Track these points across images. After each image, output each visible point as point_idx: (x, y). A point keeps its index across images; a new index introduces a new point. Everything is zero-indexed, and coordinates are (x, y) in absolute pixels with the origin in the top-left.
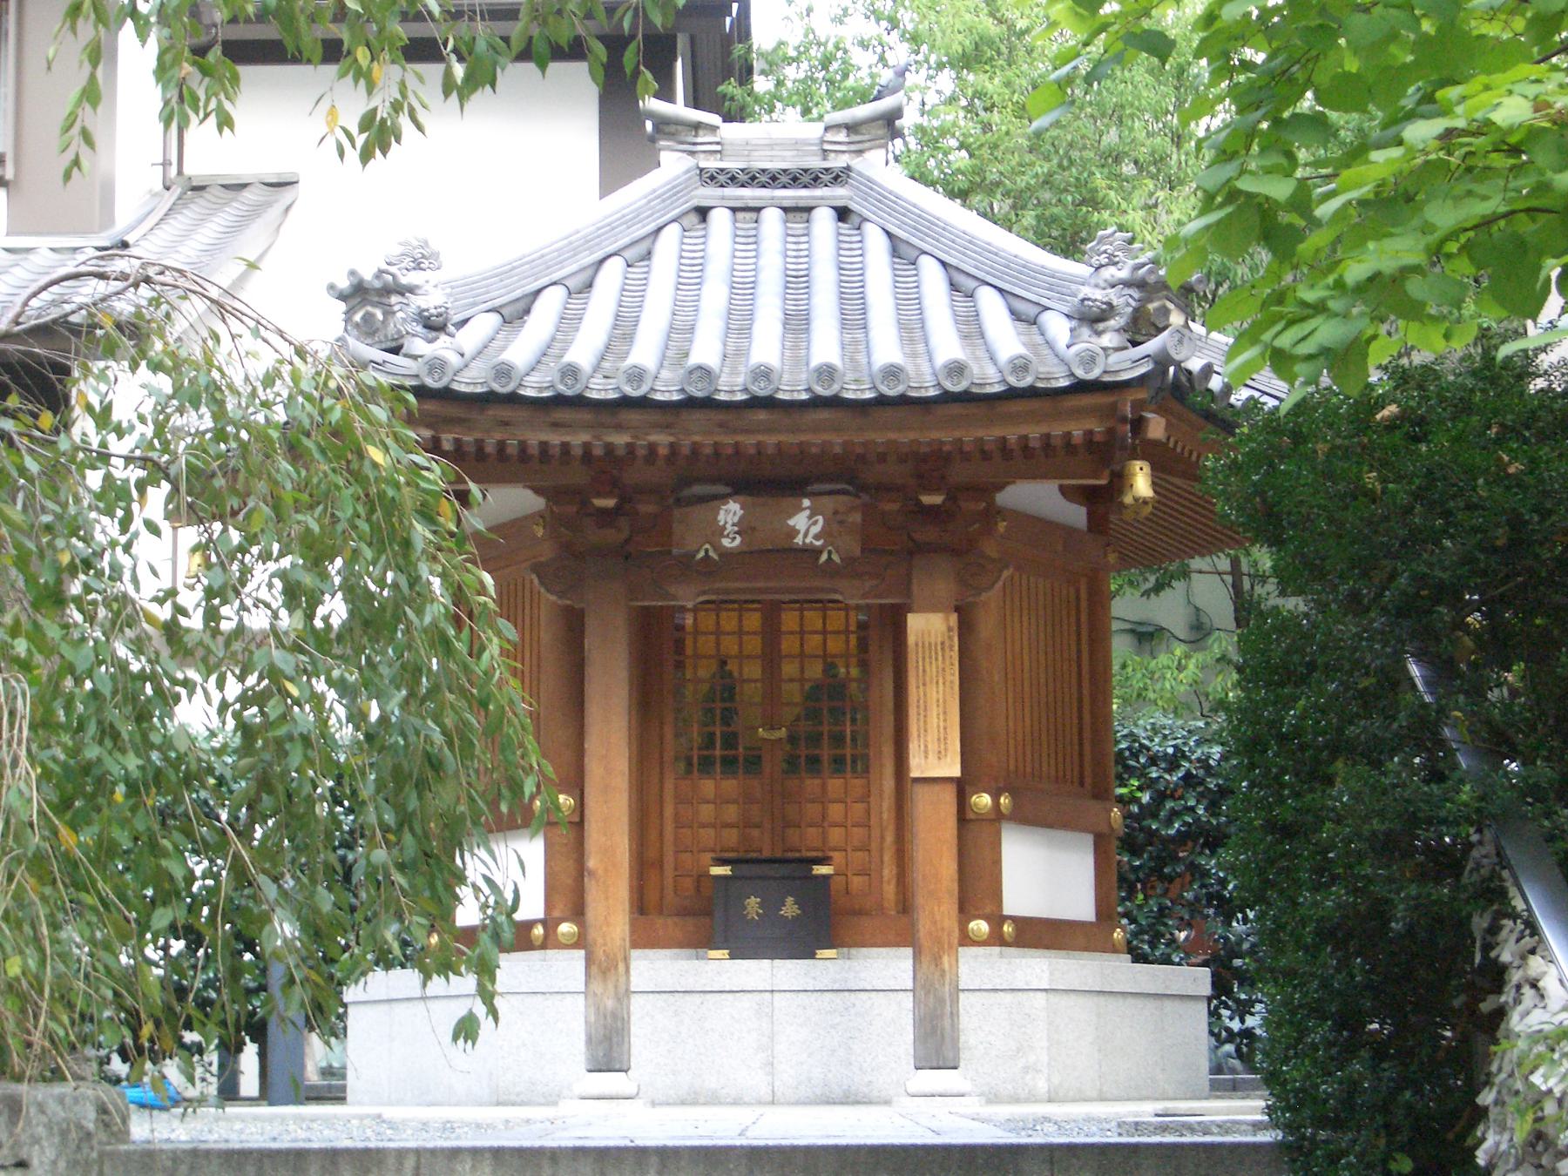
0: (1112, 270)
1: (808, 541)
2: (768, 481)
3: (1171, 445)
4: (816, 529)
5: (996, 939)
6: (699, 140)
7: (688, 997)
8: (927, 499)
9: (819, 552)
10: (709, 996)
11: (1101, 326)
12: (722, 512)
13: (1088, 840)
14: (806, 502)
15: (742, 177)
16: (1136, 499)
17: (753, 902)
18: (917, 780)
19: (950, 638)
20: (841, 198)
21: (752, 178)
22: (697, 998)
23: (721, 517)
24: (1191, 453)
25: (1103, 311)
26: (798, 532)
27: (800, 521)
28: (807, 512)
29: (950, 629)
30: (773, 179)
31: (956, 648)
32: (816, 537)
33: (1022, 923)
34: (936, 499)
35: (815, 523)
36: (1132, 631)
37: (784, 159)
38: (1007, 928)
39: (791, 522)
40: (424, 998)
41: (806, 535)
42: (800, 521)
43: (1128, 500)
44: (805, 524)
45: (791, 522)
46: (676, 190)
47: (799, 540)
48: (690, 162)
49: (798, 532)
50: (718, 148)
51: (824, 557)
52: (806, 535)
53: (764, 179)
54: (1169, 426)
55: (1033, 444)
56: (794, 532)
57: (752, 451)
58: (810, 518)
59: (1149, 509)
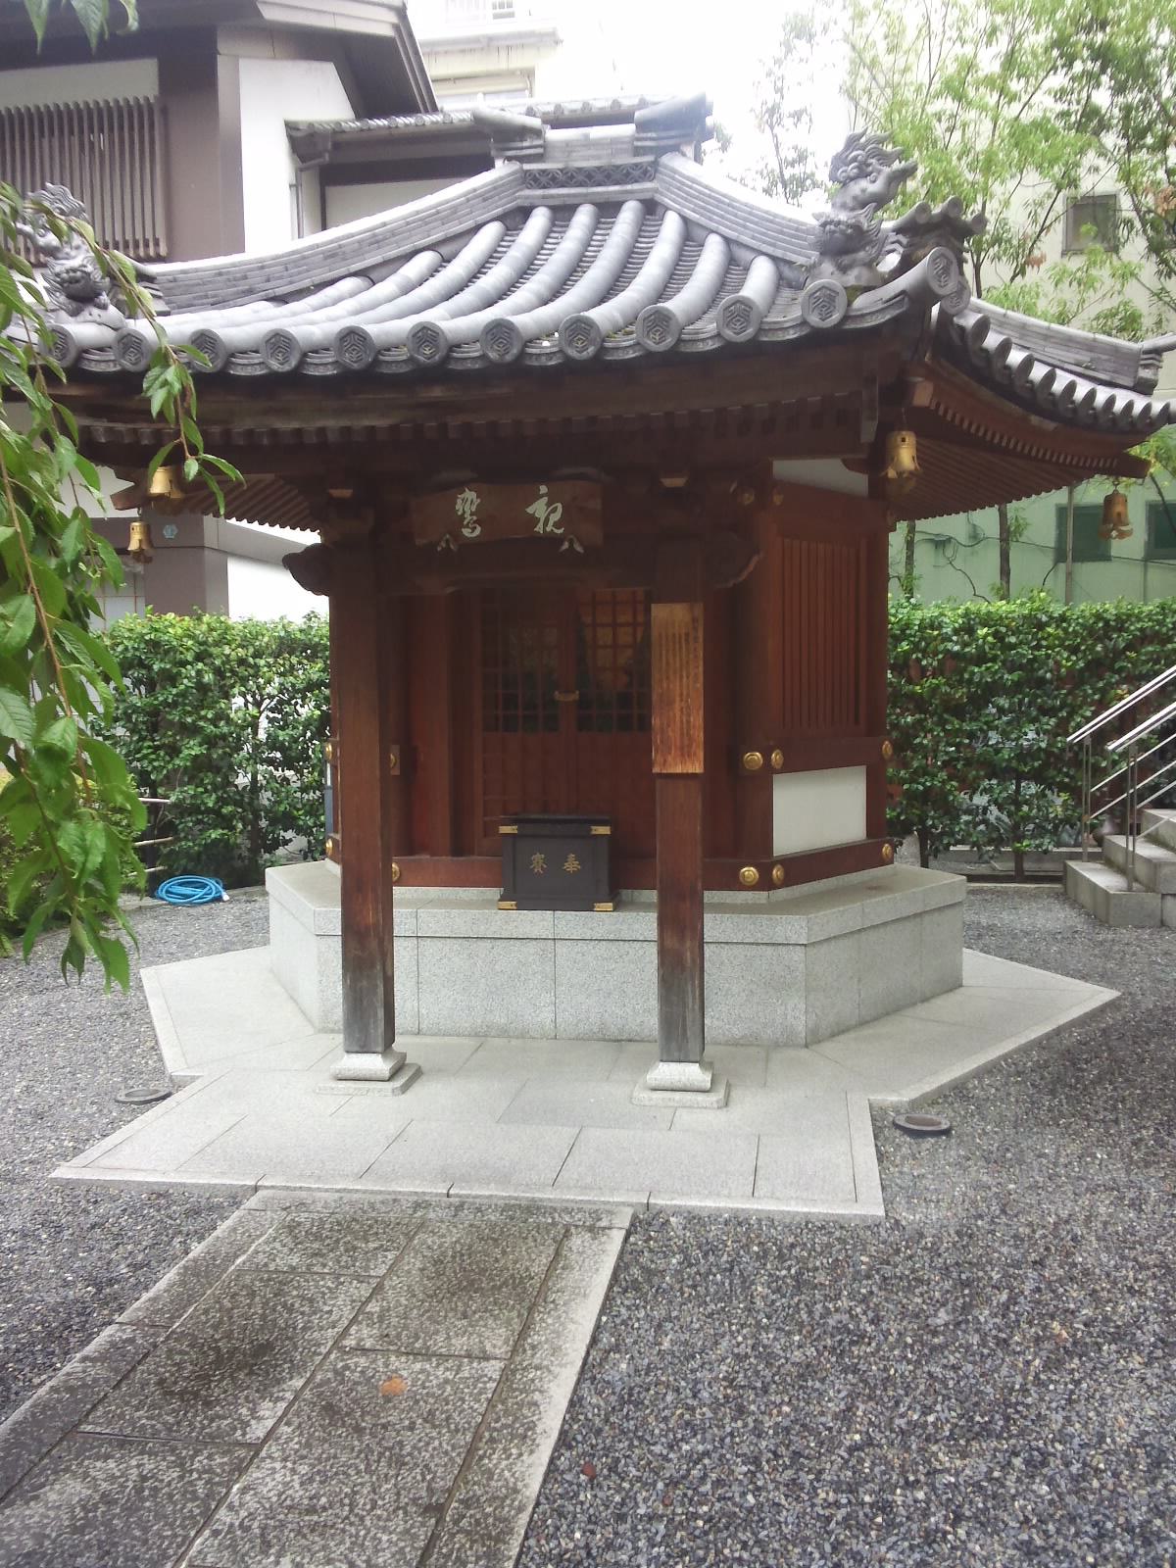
0: (864, 183)
1: (548, 529)
2: (509, 464)
3: (941, 412)
4: (556, 517)
5: (765, 884)
6: (525, 144)
7: (480, 942)
8: (670, 482)
9: (560, 540)
10: (499, 942)
11: (846, 260)
12: (459, 501)
13: (863, 769)
14: (543, 489)
15: (560, 176)
16: (900, 474)
17: (538, 858)
18: (661, 775)
19: (695, 629)
20: (647, 190)
21: (569, 178)
22: (488, 944)
23: (459, 506)
24: (962, 421)
25: (849, 237)
26: (538, 520)
27: (538, 509)
28: (545, 499)
29: (694, 620)
30: (589, 177)
31: (701, 640)
32: (557, 525)
33: (788, 862)
34: (678, 482)
35: (554, 510)
36: (931, 540)
37: (598, 157)
38: (777, 873)
39: (530, 510)
40: (1055, 366)
41: (546, 523)
42: (538, 509)
43: (892, 473)
44: (544, 512)
45: (530, 510)
46: (496, 189)
47: (539, 528)
48: (515, 166)
49: (538, 520)
50: (540, 150)
51: (566, 545)
52: (546, 523)
53: (580, 178)
54: (937, 392)
55: (332, 437)
56: (534, 520)
57: (315, 440)
58: (549, 504)
59: (912, 484)
